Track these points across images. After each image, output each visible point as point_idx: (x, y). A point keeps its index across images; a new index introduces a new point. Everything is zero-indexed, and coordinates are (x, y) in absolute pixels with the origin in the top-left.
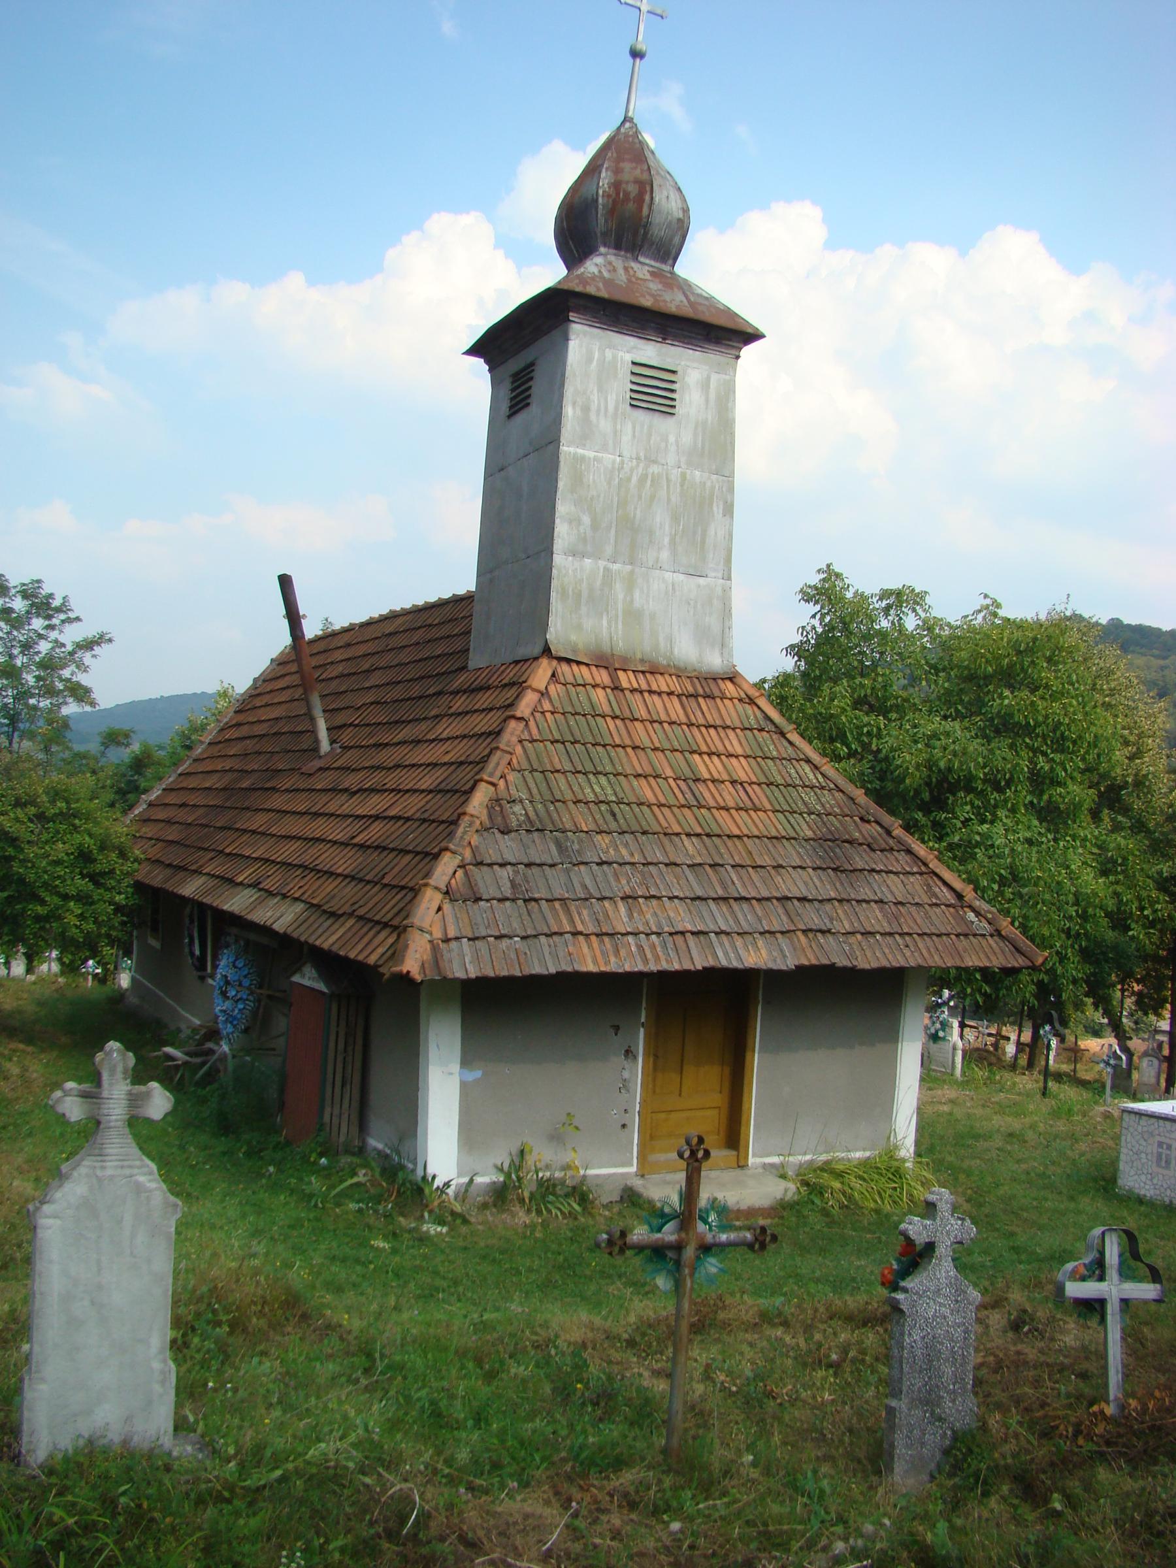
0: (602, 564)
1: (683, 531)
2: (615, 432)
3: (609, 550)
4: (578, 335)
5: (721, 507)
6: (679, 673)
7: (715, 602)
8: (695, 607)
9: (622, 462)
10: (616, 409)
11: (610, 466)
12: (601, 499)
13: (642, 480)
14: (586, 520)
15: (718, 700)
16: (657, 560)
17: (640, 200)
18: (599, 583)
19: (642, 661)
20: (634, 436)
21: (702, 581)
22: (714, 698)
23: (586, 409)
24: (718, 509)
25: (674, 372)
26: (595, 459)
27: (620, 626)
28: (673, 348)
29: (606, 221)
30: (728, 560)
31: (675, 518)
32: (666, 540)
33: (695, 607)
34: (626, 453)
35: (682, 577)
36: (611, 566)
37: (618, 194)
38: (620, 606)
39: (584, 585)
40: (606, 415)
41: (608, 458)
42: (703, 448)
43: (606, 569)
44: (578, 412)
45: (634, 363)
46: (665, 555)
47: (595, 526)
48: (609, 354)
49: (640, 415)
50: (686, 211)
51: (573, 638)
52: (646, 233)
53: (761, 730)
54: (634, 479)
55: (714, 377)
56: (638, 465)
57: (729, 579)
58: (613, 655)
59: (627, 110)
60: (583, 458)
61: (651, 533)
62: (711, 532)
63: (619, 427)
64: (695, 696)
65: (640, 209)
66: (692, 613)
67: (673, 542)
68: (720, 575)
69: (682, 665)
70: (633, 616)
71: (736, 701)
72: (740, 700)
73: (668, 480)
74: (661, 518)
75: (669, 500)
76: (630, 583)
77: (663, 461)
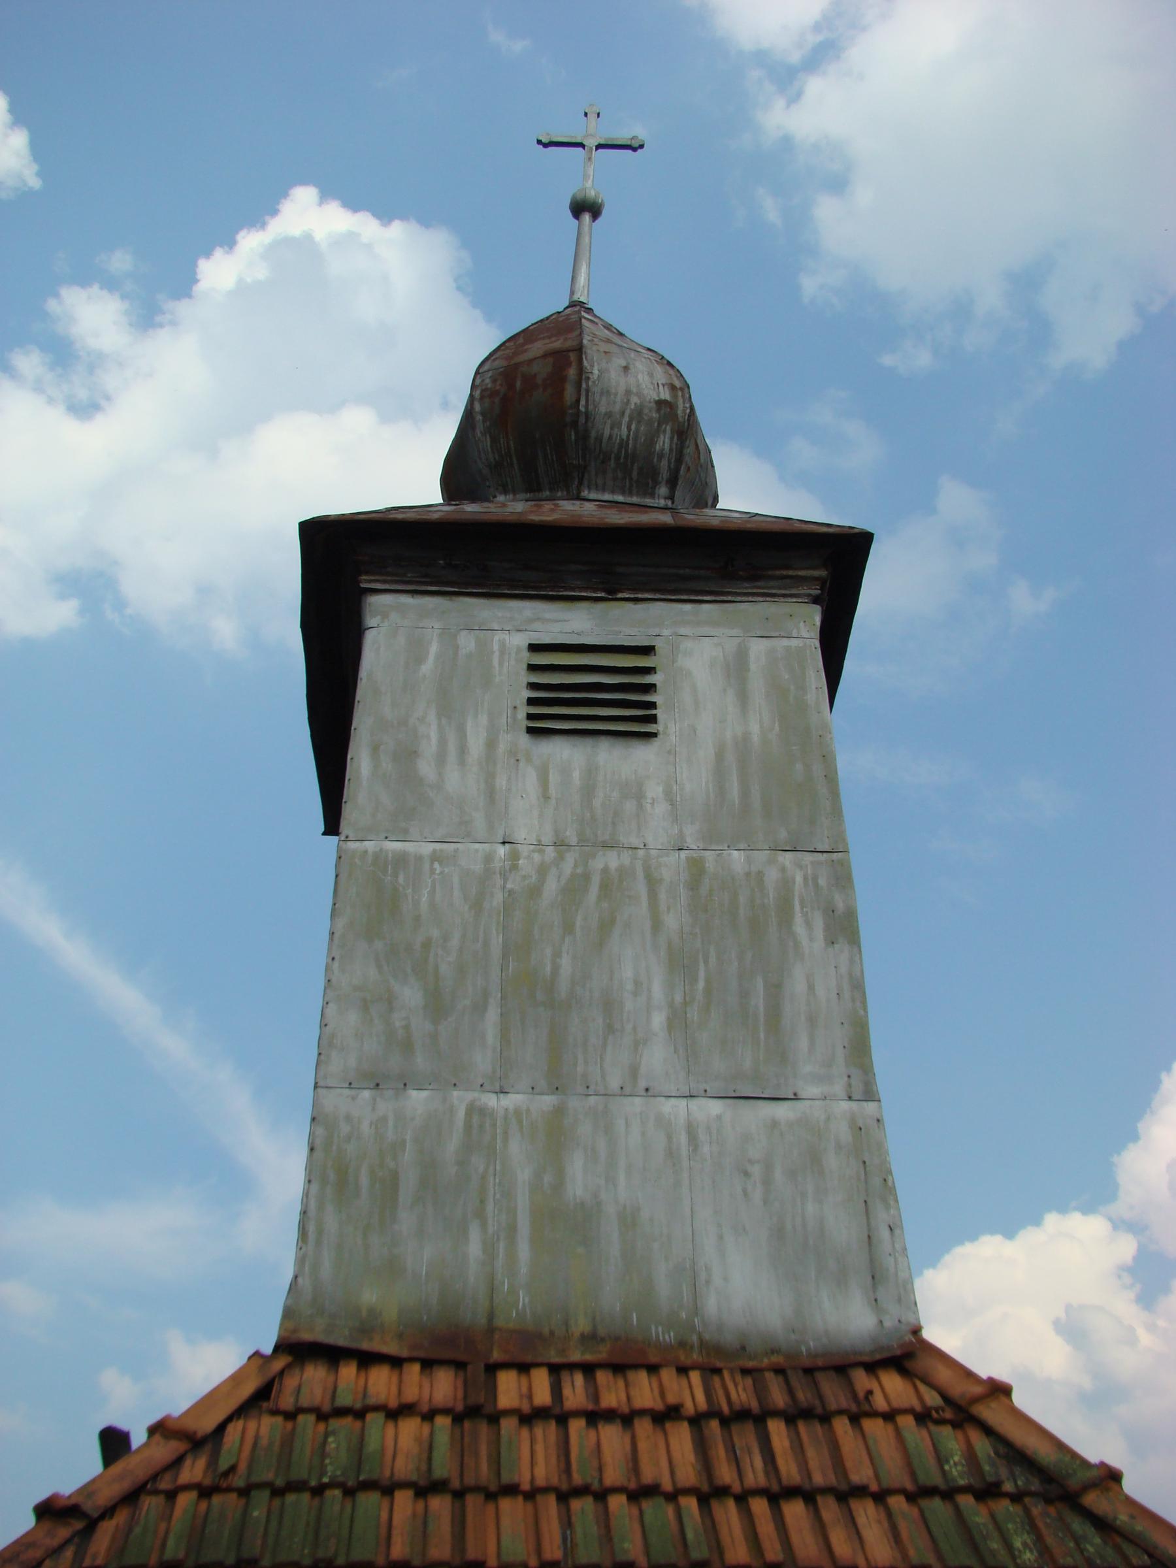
0: (460, 1099)
1: (708, 991)
2: (491, 793)
3: (482, 1061)
4: (385, 616)
5: (819, 923)
6: (713, 1359)
7: (832, 1162)
8: (767, 1182)
9: (514, 856)
10: (491, 744)
11: (478, 867)
12: (455, 942)
13: (574, 889)
14: (411, 995)
15: (841, 1426)
16: (634, 1072)
17: (557, 379)
18: (453, 1144)
19: (590, 1339)
20: (546, 797)
21: (782, 1111)
22: (826, 1418)
23: (407, 755)
24: (809, 932)
25: (648, 650)
26: (435, 857)
27: (524, 1251)
28: (639, 606)
29: (494, 440)
30: (859, 1049)
31: (680, 963)
32: (658, 1020)
33: (767, 1182)
34: (523, 834)
35: (715, 1107)
36: (491, 1101)
37: (511, 386)
38: (523, 1201)
39: (408, 1156)
40: (462, 762)
41: (471, 854)
42: (745, 794)
43: (471, 1109)
44: (387, 765)
45: (534, 648)
46: (658, 1058)
47: (437, 1005)
48: (467, 642)
49: (564, 753)
50: (681, 388)
51: (369, 1296)
52: (584, 437)
53: (987, 1492)
54: (551, 887)
55: (758, 649)
56: (561, 857)
57: (870, 1095)
58: (491, 1330)
59: (572, 293)
60: (401, 860)
61: (609, 1006)
62: (797, 984)
63: (501, 782)
64: (759, 1418)
65: (560, 393)
66: (757, 1195)
67: (677, 1021)
68: (839, 1088)
69: (729, 1339)
70: (566, 1224)
71: (907, 1422)
72: (923, 1417)
73: (652, 883)
74: (638, 971)
75: (657, 925)
76: (555, 1137)
77: (634, 841)
